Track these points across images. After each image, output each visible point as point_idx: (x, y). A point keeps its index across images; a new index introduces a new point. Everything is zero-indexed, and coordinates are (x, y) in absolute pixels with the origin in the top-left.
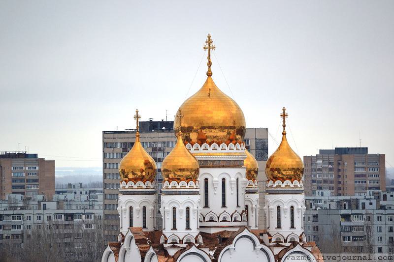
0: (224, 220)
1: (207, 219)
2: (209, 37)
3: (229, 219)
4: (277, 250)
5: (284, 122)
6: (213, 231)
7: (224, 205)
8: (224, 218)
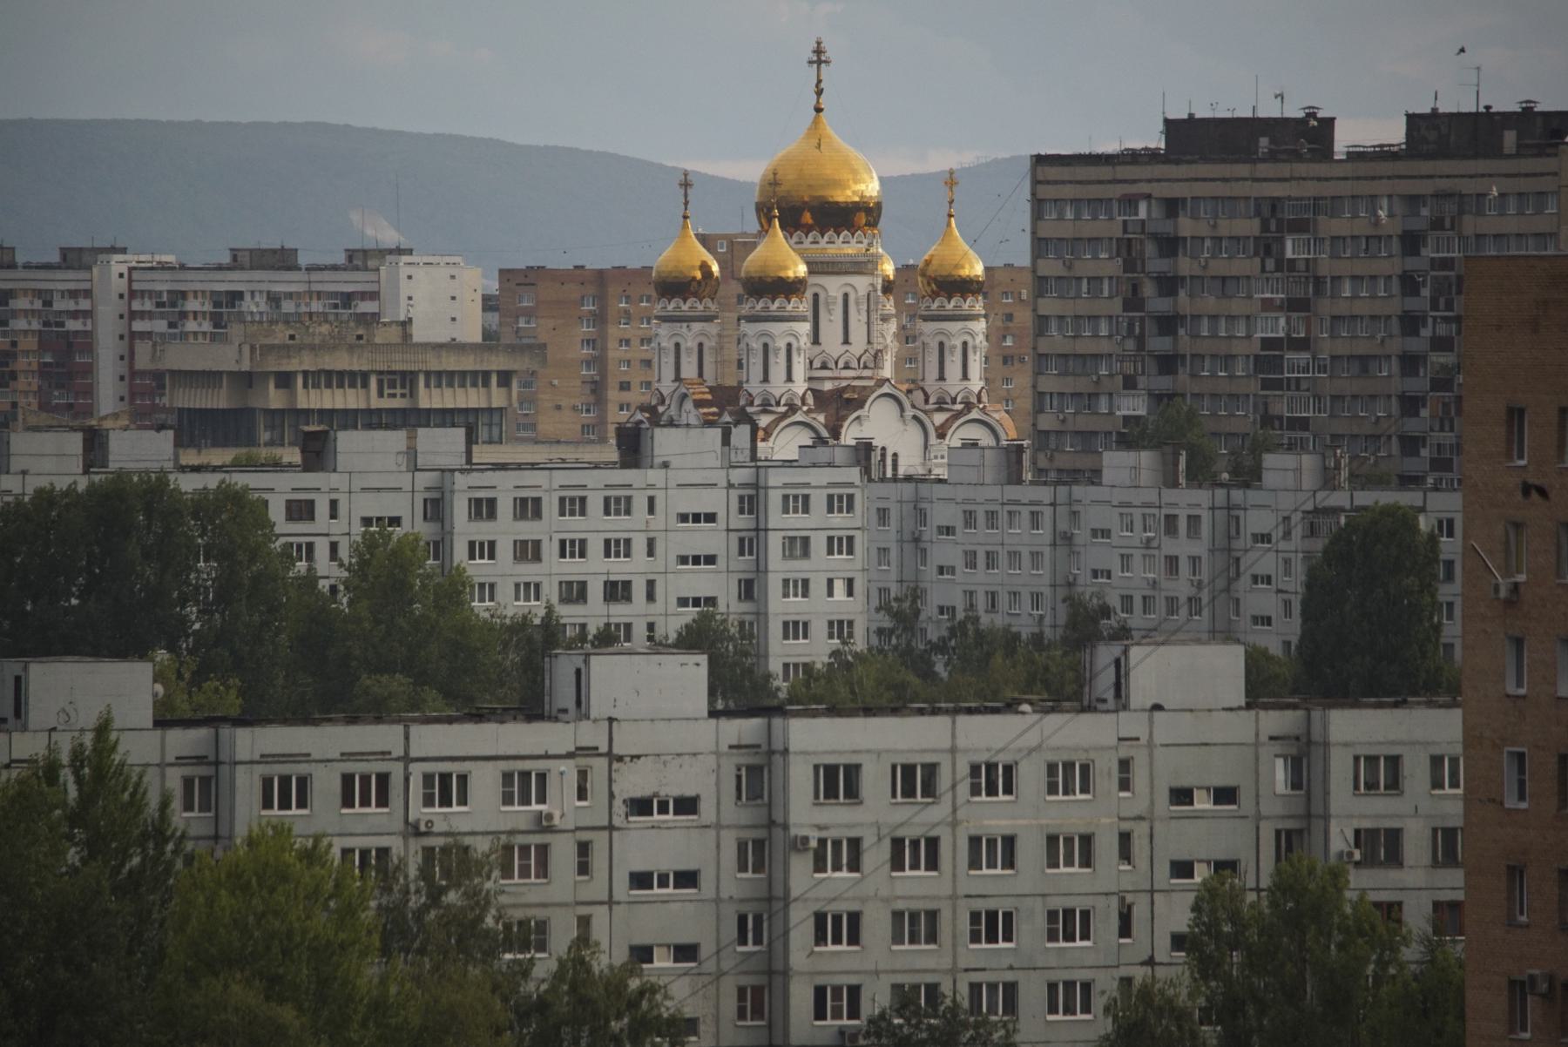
0: (847, 367)
1: (817, 364)
2: (819, 43)
3: (854, 364)
4: (939, 418)
5: (686, 195)
6: (828, 386)
7: (846, 341)
8: (846, 363)
